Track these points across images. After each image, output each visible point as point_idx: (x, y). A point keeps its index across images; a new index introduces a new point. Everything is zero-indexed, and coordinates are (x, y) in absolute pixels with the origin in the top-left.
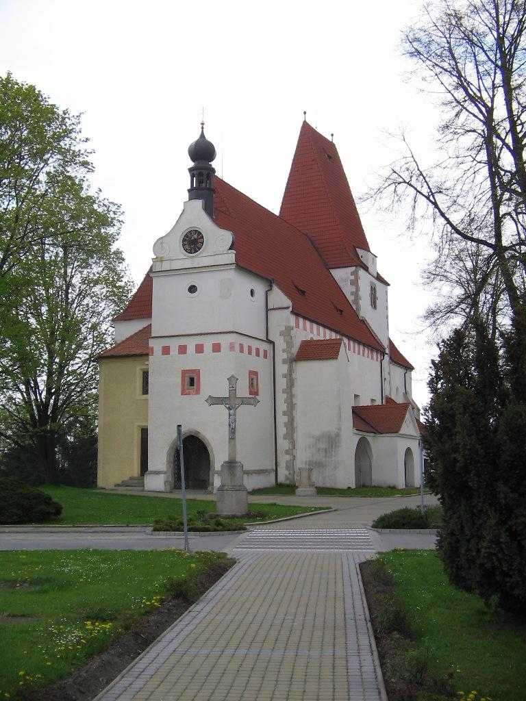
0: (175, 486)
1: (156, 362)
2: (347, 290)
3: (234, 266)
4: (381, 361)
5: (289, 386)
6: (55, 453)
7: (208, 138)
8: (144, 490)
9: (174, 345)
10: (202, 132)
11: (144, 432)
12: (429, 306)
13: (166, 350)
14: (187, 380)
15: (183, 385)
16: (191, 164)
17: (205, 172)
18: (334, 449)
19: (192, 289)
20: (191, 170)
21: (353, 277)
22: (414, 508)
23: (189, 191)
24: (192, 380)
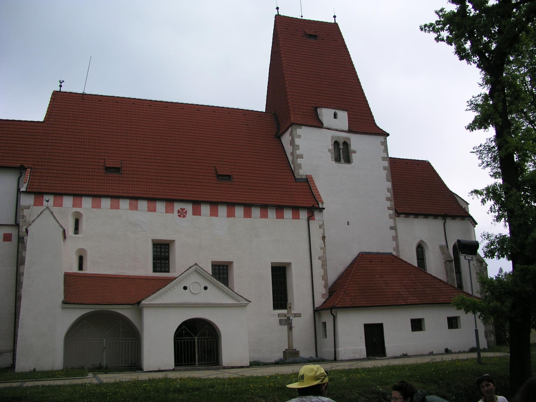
12: (385, 168)
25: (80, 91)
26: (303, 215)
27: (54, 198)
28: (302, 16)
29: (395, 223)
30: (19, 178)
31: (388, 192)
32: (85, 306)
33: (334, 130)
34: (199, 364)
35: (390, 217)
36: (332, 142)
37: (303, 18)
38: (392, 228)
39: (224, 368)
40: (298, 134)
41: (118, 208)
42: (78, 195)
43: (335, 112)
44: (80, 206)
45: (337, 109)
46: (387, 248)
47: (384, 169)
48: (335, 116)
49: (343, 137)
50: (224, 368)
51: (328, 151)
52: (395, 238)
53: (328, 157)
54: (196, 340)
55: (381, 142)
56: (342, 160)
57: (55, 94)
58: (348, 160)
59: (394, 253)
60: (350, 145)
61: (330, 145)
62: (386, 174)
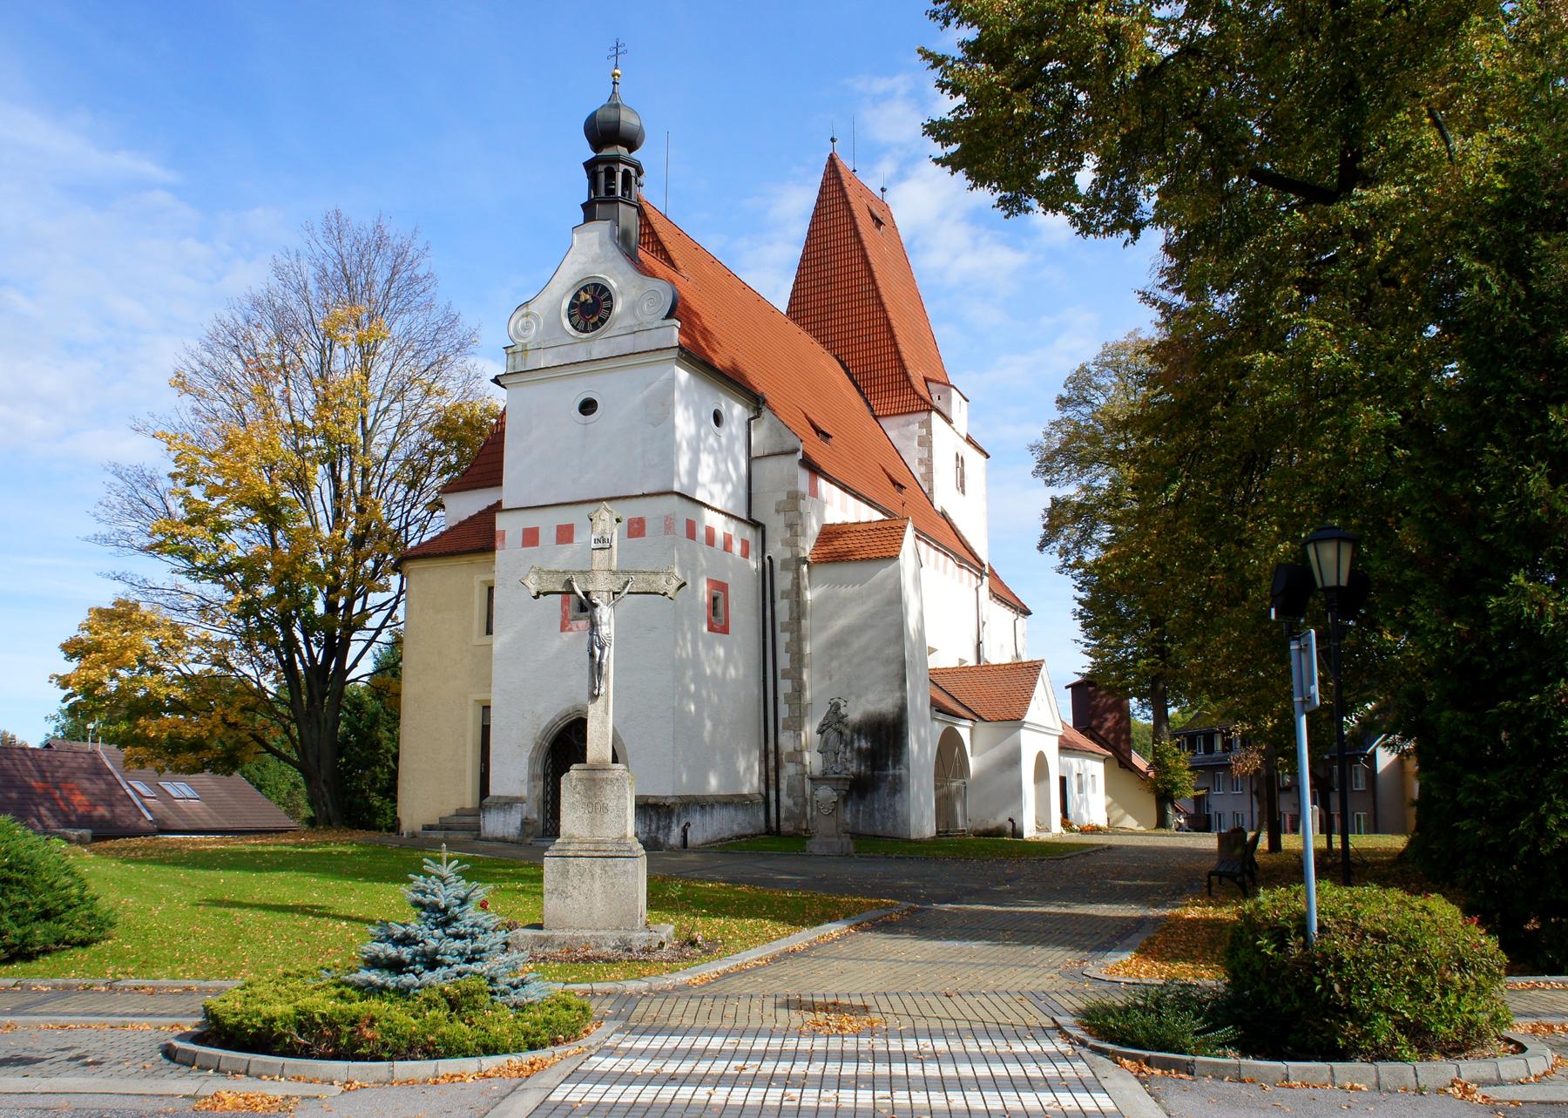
1: (509, 553)
2: (912, 456)
3: (674, 354)
4: (977, 589)
5: (795, 615)
8: (478, 838)
9: (547, 523)
11: (486, 709)
13: (531, 537)
15: (565, 614)
18: (891, 751)
19: (588, 407)
21: (924, 431)
22: (110, 607)
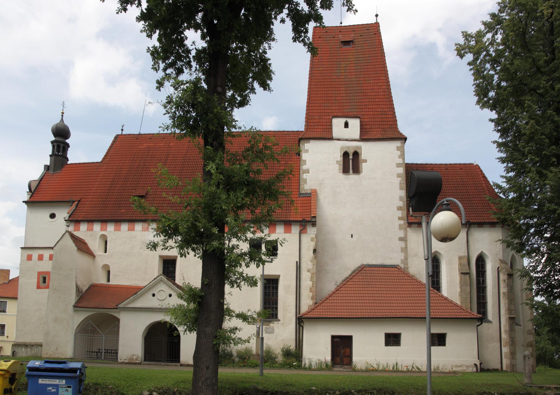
0: (171, 277)
6: (494, 189)
7: (66, 122)
10: (62, 119)
12: (399, 176)
14: (41, 280)
16: (53, 138)
17: (62, 145)
20: (52, 142)
23: (51, 156)
24: (45, 278)
25: (136, 132)
26: (296, 229)
27: (115, 226)
28: (341, 23)
29: (406, 235)
30: (467, 232)
31: (400, 200)
32: (88, 309)
33: (344, 140)
34: (104, 358)
35: (400, 227)
36: (341, 152)
37: (343, 25)
38: (401, 239)
39: (181, 365)
40: (306, 148)
41: (133, 230)
42: (104, 221)
43: (346, 121)
44: (106, 230)
45: (348, 117)
46: (395, 259)
47: (398, 177)
48: (346, 125)
49: (353, 147)
50: (181, 365)
51: (335, 162)
52: (405, 250)
53: (336, 168)
54: (104, 338)
55: (397, 147)
56: (351, 171)
57: (117, 137)
58: (357, 170)
59: (402, 266)
60: (361, 154)
61: (339, 157)
62: (400, 182)
